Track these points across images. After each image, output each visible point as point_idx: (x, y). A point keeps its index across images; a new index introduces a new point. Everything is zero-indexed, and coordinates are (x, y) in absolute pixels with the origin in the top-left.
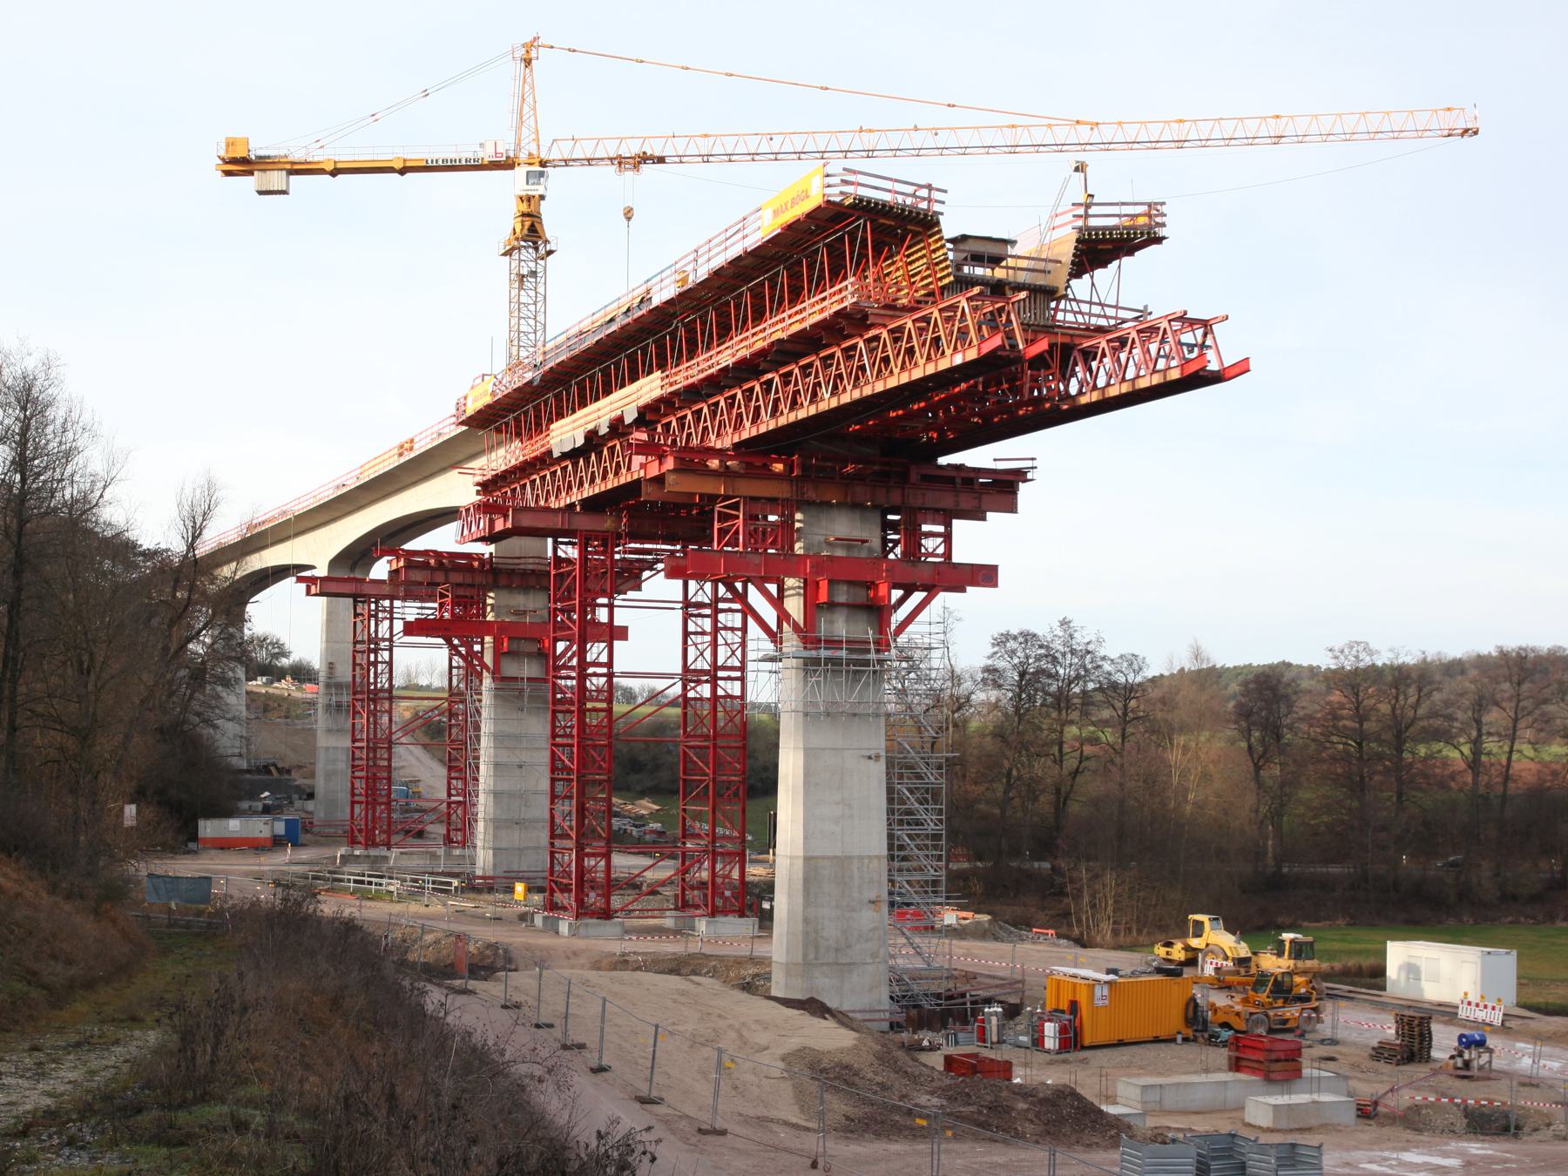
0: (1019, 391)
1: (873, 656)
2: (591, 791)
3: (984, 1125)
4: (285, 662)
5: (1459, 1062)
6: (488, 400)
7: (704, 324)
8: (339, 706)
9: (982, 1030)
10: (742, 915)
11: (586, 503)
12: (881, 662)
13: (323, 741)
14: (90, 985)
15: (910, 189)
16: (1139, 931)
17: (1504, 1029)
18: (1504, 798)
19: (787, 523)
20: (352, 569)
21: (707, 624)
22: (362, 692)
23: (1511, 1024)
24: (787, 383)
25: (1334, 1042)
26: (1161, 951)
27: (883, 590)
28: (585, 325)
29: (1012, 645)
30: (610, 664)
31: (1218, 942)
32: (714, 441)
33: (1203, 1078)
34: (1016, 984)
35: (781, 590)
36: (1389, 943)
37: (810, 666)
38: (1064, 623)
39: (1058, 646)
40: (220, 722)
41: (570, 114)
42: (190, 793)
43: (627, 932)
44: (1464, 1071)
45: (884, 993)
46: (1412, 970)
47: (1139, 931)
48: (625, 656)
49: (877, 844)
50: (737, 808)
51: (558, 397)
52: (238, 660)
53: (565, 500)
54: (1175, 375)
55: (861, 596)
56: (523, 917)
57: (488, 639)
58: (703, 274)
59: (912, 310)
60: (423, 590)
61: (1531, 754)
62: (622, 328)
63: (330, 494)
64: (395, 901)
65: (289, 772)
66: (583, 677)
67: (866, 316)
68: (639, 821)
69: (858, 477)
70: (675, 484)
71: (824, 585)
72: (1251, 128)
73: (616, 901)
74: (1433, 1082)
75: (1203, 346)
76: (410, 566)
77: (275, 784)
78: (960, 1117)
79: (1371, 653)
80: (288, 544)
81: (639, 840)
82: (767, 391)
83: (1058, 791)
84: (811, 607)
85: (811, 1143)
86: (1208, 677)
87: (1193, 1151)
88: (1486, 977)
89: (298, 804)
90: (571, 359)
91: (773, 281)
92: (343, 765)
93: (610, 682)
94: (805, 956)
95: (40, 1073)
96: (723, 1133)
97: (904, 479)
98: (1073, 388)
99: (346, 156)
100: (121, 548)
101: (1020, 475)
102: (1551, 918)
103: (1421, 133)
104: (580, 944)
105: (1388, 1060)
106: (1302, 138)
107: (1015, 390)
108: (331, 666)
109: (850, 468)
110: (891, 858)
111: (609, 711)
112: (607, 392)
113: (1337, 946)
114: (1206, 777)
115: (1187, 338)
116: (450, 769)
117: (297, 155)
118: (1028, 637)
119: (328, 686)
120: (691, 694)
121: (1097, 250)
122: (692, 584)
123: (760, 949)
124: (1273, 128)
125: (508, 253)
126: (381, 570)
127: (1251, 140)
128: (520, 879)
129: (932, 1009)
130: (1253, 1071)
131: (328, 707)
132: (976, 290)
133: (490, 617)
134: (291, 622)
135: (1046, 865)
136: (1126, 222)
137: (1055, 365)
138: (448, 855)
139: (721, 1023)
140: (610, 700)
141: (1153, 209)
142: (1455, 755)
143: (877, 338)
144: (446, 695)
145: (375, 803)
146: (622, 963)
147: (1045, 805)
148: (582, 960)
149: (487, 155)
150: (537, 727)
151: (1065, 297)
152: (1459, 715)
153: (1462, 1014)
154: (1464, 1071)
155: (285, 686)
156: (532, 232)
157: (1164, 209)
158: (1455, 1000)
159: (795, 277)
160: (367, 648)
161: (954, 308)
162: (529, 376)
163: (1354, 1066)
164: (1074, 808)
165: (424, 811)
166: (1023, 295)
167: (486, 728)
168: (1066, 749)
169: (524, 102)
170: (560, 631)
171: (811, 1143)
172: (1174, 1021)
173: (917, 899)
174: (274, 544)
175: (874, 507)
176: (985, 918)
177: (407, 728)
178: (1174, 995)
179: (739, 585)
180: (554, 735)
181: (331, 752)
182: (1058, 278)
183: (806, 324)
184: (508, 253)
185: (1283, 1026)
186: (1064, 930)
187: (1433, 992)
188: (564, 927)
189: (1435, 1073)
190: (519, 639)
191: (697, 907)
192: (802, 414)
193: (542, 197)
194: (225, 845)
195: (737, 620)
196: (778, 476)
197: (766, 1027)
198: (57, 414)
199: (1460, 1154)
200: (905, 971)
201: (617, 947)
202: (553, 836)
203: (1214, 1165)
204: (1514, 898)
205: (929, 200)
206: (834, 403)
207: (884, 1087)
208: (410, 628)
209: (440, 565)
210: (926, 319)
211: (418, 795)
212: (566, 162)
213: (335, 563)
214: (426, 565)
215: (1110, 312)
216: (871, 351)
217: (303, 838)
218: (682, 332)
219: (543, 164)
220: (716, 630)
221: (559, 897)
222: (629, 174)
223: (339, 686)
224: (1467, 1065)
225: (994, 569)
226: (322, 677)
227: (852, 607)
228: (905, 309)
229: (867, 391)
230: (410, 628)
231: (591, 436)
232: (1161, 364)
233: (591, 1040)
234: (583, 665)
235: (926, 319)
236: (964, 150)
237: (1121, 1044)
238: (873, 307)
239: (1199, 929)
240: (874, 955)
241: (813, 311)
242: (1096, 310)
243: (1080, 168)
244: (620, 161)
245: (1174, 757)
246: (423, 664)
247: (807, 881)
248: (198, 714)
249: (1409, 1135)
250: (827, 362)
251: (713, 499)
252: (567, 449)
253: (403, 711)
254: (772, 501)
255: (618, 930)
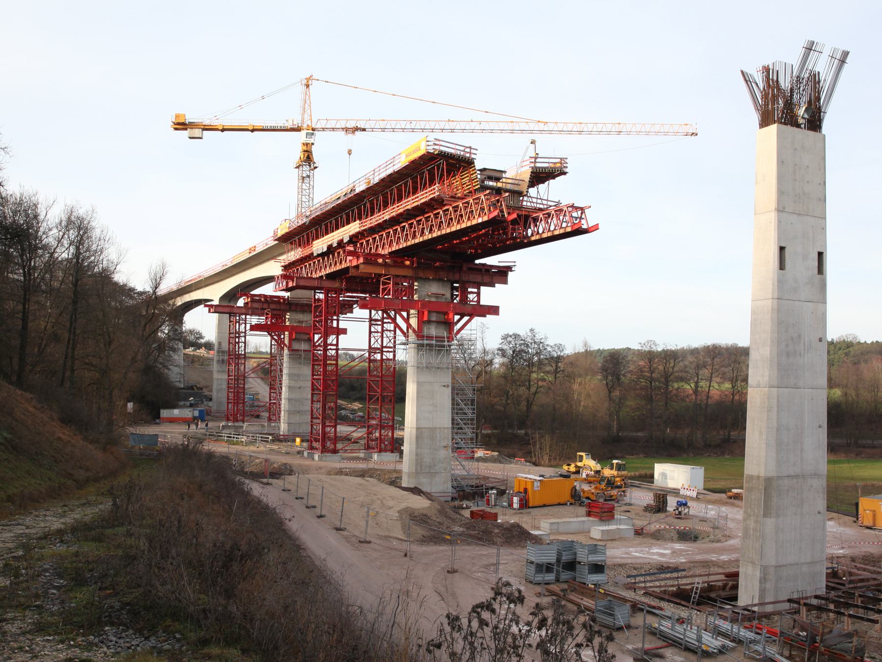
0: (506, 234)
1: (446, 343)
2: (329, 399)
3: (480, 539)
4: (202, 341)
5: (677, 512)
6: (287, 230)
7: (377, 201)
8: (223, 361)
9: (488, 500)
10: (392, 452)
11: (328, 276)
12: (449, 346)
13: (216, 376)
14: (96, 480)
15: (462, 148)
16: (560, 460)
17: (697, 499)
18: (707, 405)
19: (411, 287)
20: (230, 301)
21: (379, 328)
22: (233, 356)
23: (700, 496)
24: (411, 228)
25: (630, 504)
26: (565, 467)
27: (451, 316)
28: (327, 200)
29: (509, 339)
30: (337, 345)
31: (589, 464)
32: (381, 251)
33: (572, 520)
34: (504, 481)
35: (408, 315)
36: (656, 465)
37: (420, 347)
38: (532, 330)
39: (529, 340)
40: (171, 367)
41: (326, 107)
42: (156, 397)
43: (343, 459)
44: (679, 516)
45: (449, 485)
46: (664, 475)
47: (560, 460)
48: (344, 342)
49: (449, 424)
50: (391, 407)
51: (317, 230)
52: (179, 340)
53: (319, 274)
54: (569, 230)
55: (442, 318)
56: (299, 453)
57: (286, 333)
58: (376, 180)
59: (462, 199)
60: (260, 312)
61: (717, 387)
62: (343, 202)
63: (220, 269)
64: (243, 446)
65: (202, 389)
66: (325, 350)
67: (443, 201)
68: (354, 411)
69: (441, 268)
70: (363, 269)
71: (426, 313)
72: (609, 128)
73: (339, 446)
74: (667, 520)
75: (581, 218)
76: (253, 301)
77: (195, 394)
78: (471, 536)
79: (656, 345)
80: (201, 290)
81: (353, 420)
82: (403, 231)
83: (528, 401)
84: (421, 322)
85: (405, 546)
86: (588, 354)
87: (556, 548)
88: (692, 478)
89: (205, 403)
90: (322, 214)
91: (406, 184)
92: (225, 386)
93: (337, 353)
94: (416, 469)
95: (63, 516)
96: (369, 542)
97: (460, 269)
98: (530, 232)
99: (228, 123)
100: (126, 291)
101: (510, 268)
102: (723, 454)
103: (676, 133)
104: (322, 464)
105: (650, 512)
106: (629, 133)
107: (506, 233)
108: (220, 343)
109: (437, 264)
110: (453, 428)
111: (337, 365)
112: (337, 229)
113: (639, 465)
114: (588, 396)
115: (575, 214)
116: (271, 388)
117: (207, 122)
118: (516, 336)
119: (218, 352)
120: (372, 358)
121: (540, 176)
122: (373, 312)
123: (398, 467)
124: (617, 128)
125: (298, 167)
126: (241, 303)
127: (609, 133)
128: (298, 436)
129: (470, 491)
130: (596, 516)
131: (218, 361)
132: (488, 192)
133: (287, 324)
134: (202, 323)
135: (523, 432)
136: (552, 165)
137: (522, 223)
138: (269, 426)
139: (375, 497)
140: (337, 361)
141: (563, 160)
142: (689, 388)
143: (448, 210)
144: (269, 356)
145: (238, 403)
146: (340, 472)
147: (520, 407)
148: (323, 471)
149: (289, 125)
150: (306, 371)
151: (526, 195)
152: (691, 371)
153: (681, 492)
154: (679, 516)
155: (202, 352)
156: (308, 158)
157: (567, 161)
158: (679, 486)
159: (415, 183)
160: (235, 336)
161: (478, 198)
162: (305, 220)
163: (637, 514)
164: (535, 408)
165: (259, 406)
166: (507, 194)
167: (285, 371)
168: (532, 383)
169: (306, 103)
170: (316, 330)
171: (405, 546)
172: (566, 496)
173: (464, 446)
174: (195, 290)
175: (448, 281)
176: (496, 454)
177: (254, 370)
178: (567, 485)
179: (392, 313)
180: (313, 375)
181: (219, 381)
182: (523, 187)
183: (419, 203)
184: (298, 167)
185: (611, 498)
186: (529, 459)
187: (671, 484)
188: (316, 457)
189: (667, 516)
190: (301, 334)
191: (374, 449)
192: (417, 241)
193: (313, 144)
194: (172, 420)
195: (392, 327)
196: (407, 267)
197: (393, 498)
198: (96, 233)
199: (671, 548)
200: (459, 476)
201: (338, 465)
202: (312, 418)
203: (564, 553)
204: (710, 446)
205: (470, 153)
206: (430, 237)
207: (440, 523)
208: (254, 328)
209: (266, 301)
210: (468, 203)
211: (258, 400)
212: (323, 129)
213: (222, 299)
214: (260, 301)
215: (545, 202)
216: (445, 215)
217: (207, 418)
218: (368, 205)
219: (313, 130)
220: (383, 331)
221: (315, 444)
222: (350, 135)
223: (223, 352)
224: (680, 513)
225: (498, 307)
226: (216, 347)
227: (438, 323)
228: (460, 198)
229: (444, 232)
230: (254, 328)
231: (330, 247)
232: (564, 225)
233: (318, 504)
234: (326, 345)
235: (468, 203)
236: (492, 131)
237: (545, 506)
238: (446, 197)
239: (581, 460)
240: (445, 469)
241: (410, 203)
242: (539, 201)
243: (533, 142)
244: (346, 130)
245: (575, 387)
246: (259, 343)
247: (417, 438)
248: (161, 363)
249: (653, 541)
250: (427, 219)
251: (380, 275)
252: (320, 252)
253: (251, 364)
254: (405, 277)
255: (339, 458)
